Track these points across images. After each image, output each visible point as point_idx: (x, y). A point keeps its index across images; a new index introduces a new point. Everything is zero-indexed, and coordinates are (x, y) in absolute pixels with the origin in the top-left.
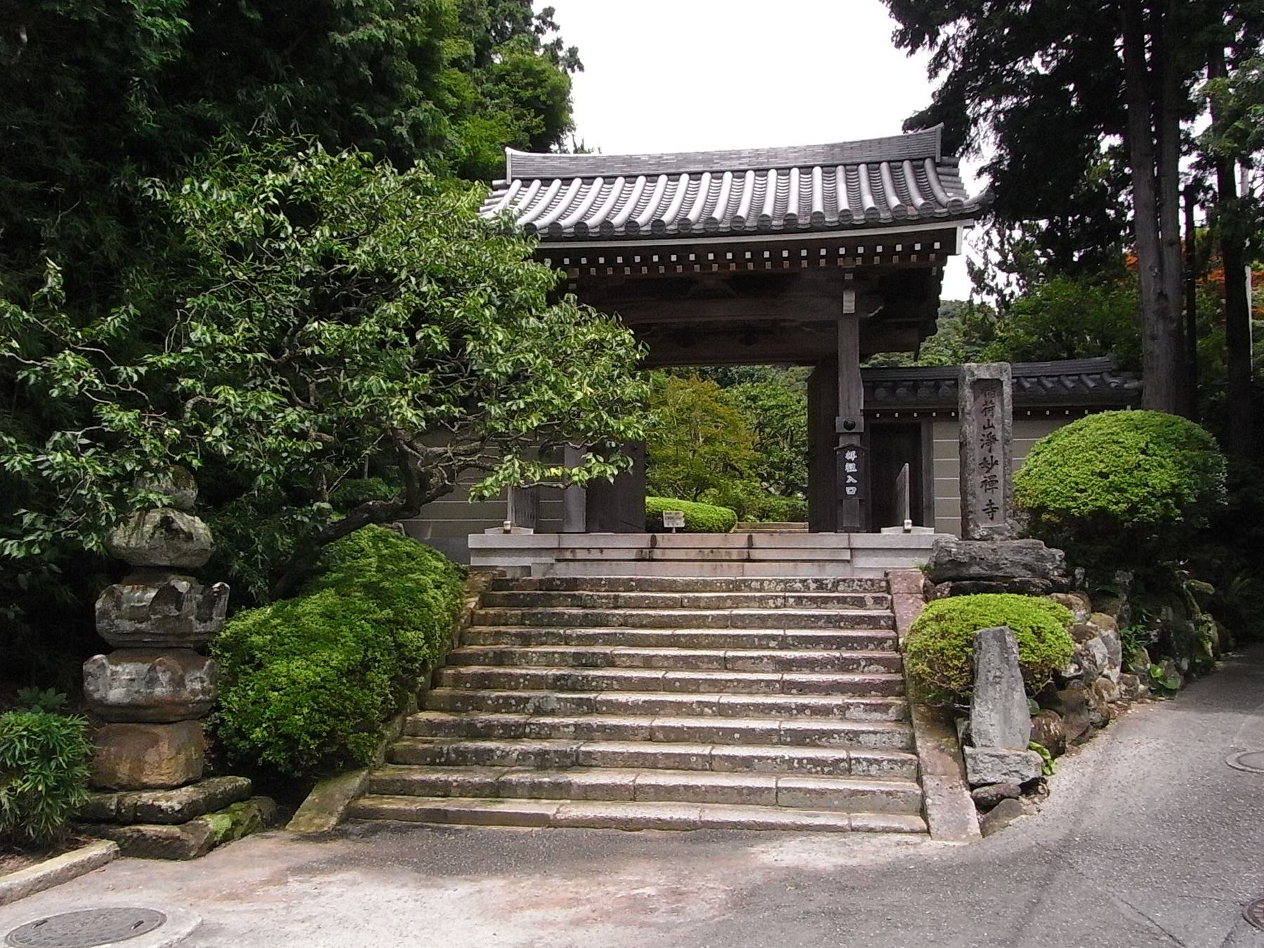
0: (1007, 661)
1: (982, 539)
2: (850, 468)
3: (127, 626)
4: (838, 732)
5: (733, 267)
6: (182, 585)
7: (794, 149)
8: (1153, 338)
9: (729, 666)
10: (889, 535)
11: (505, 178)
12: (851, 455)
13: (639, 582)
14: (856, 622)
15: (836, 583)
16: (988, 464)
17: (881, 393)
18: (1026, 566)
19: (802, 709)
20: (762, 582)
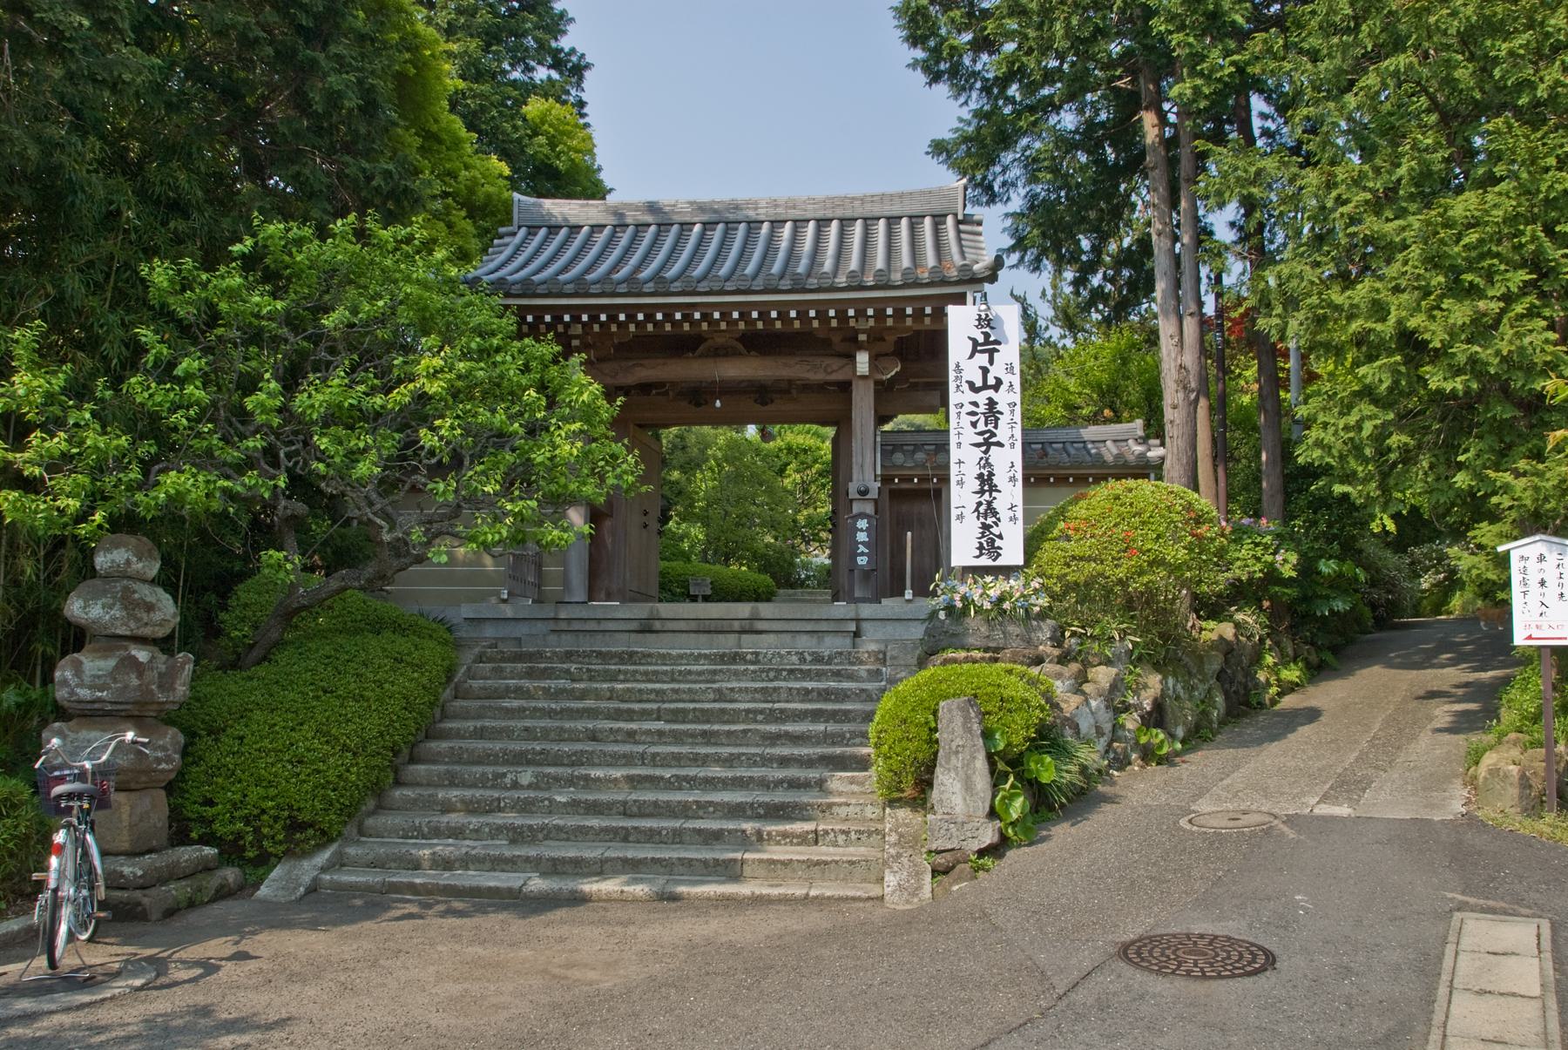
3: (84, 693)
5: (742, 325)
6: (142, 655)
7: (813, 201)
8: (1175, 407)
10: (890, 605)
13: (631, 655)
17: (898, 458)
20: (757, 654)
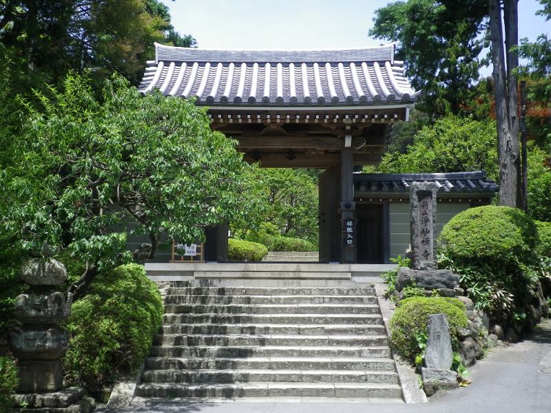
0: (443, 328)
1: (422, 269)
2: (349, 230)
4: (359, 363)
9: (301, 332)
11: (154, 60)
12: (350, 223)
14: (360, 310)
15: (348, 291)
16: (425, 232)
18: (443, 283)
19: (340, 352)
